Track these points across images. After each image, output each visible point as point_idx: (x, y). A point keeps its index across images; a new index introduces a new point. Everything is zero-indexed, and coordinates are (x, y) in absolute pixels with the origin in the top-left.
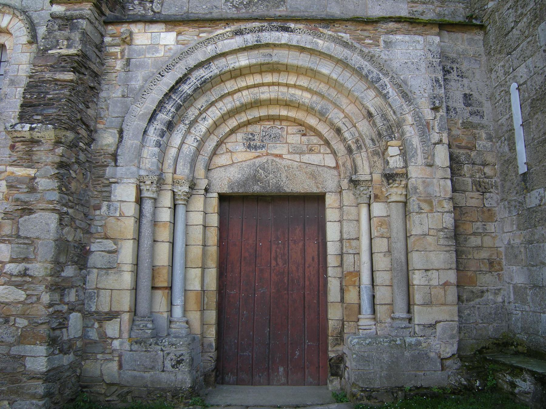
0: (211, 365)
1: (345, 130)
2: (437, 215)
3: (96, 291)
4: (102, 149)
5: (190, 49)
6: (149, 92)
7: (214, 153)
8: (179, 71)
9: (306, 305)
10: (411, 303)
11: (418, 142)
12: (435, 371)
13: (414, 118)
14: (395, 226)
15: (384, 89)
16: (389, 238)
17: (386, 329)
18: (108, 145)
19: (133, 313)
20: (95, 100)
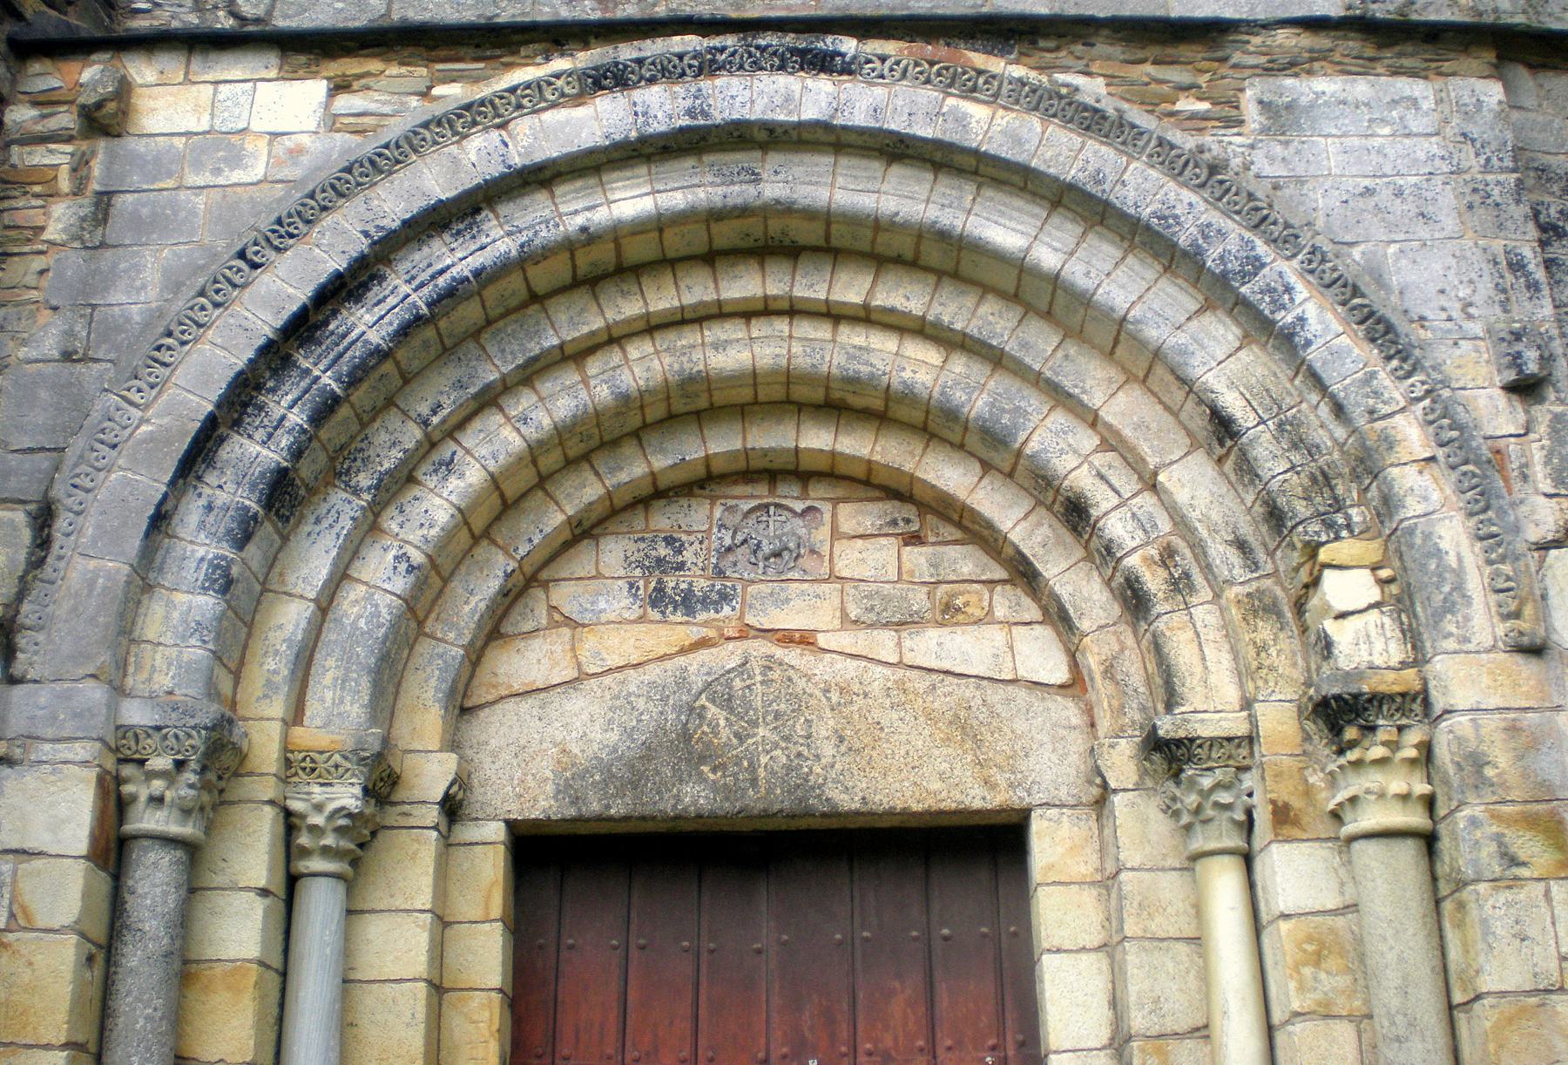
1: (1105, 506)
5: (386, 146)
6: (186, 337)
8: (331, 245)
13: (1431, 429)
14: (1391, 957)
15: (1283, 307)
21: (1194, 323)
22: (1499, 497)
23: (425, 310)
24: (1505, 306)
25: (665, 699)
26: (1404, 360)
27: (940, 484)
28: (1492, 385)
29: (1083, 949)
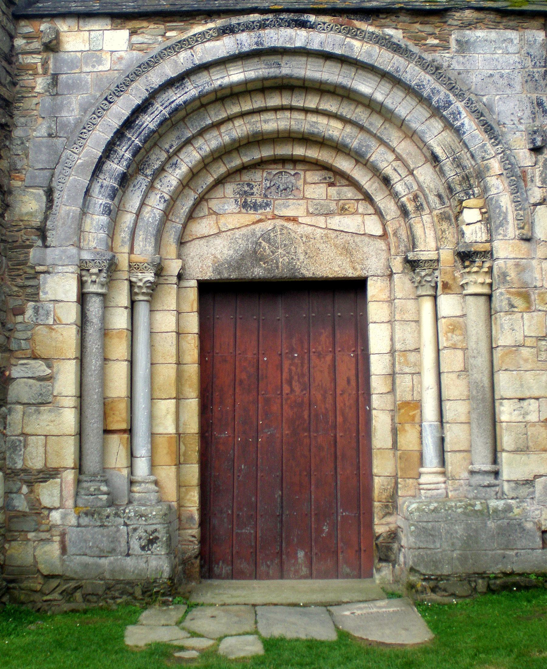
0: (194, 548)
1: (396, 180)
2: (537, 316)
3: (21, 438)
4: (22, 221)
5: (152, 57)
6: (90, 129)
7: (191, 217)
8: (136, 94)
9: (338, 454)
10: (499, 449)
11: (509, 203)
12: (533, 549)
13: (502, 164)
14: (474, 332)
15: (457, 120)
16: (465, 350)
17: (461, 489)
18: (31, 214)
19: (78, 470)
20: (7, 143)
21: (428, 122)
22: (522, 189)
23: (168, 116)
24: (534, 119)
25: (248, 240)
26: (496, 140)
27: (341, 168)
28: (525, 148)
29: (383, 322)
